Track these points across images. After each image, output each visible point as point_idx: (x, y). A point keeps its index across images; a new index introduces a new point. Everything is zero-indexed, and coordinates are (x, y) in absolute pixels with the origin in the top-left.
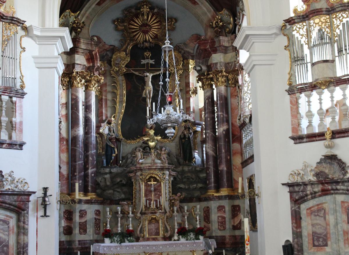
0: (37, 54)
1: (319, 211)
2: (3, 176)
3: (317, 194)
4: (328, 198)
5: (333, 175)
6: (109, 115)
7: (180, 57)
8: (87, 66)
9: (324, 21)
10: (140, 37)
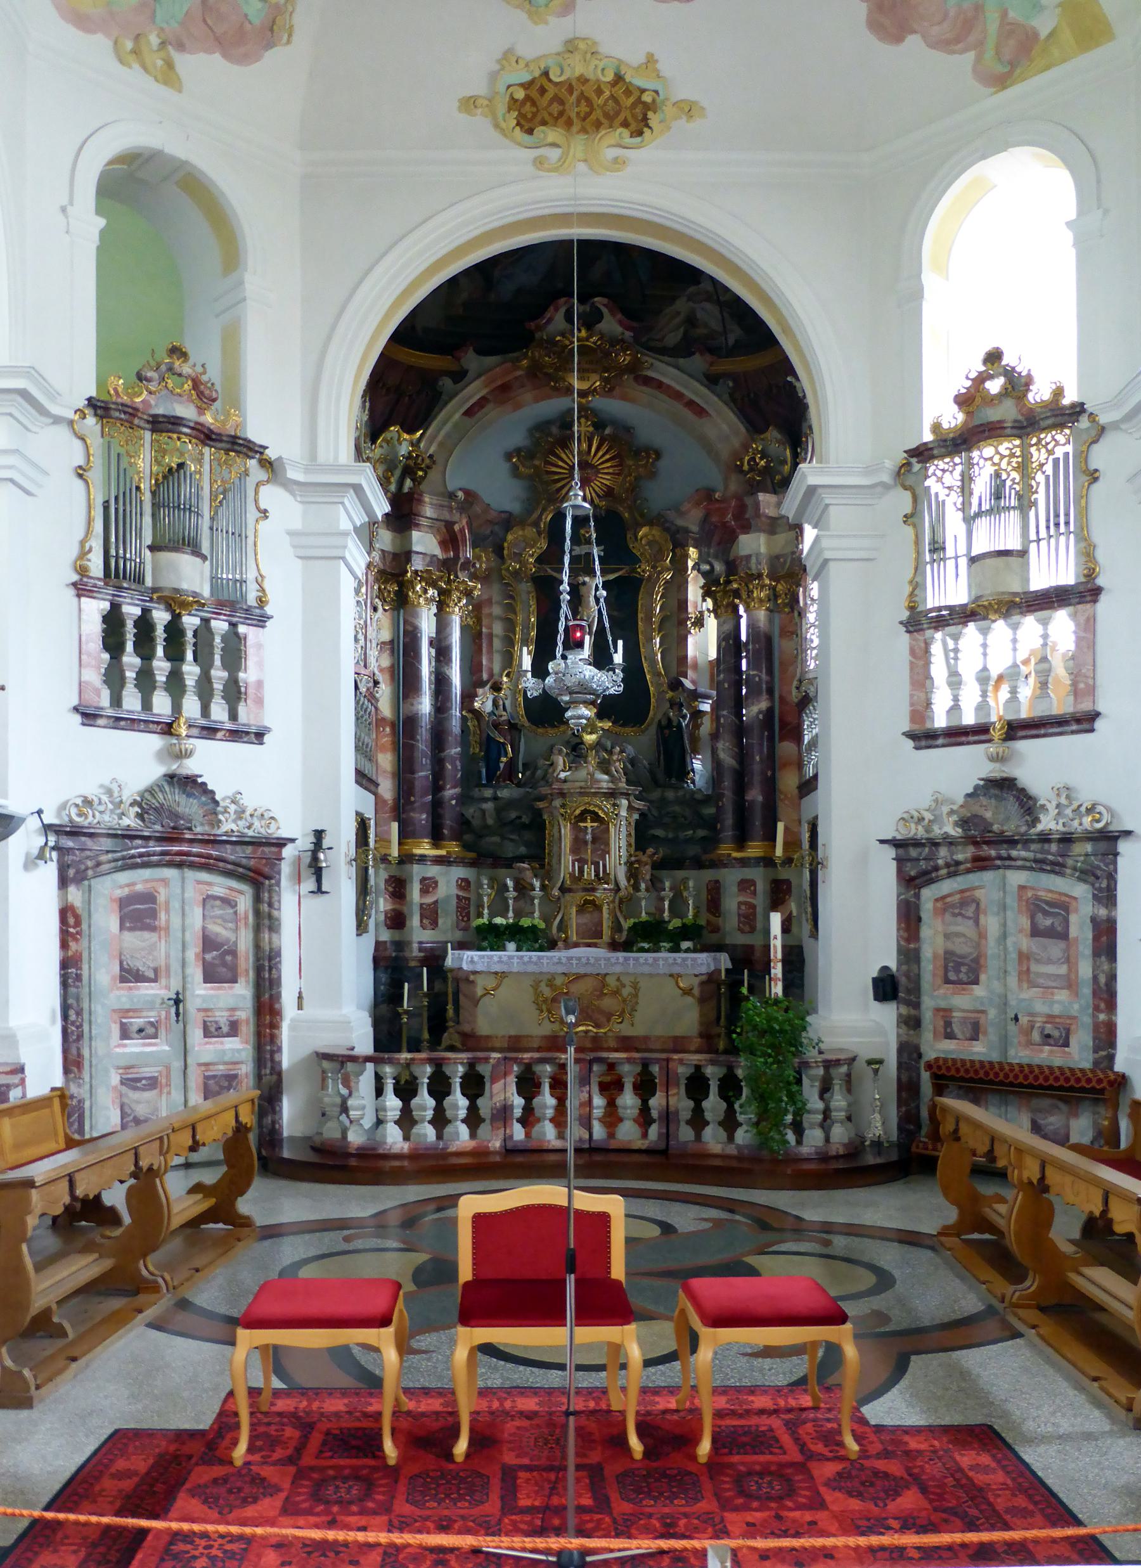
0: (297, 525)
2: (217, 803)
3: (962, 867)
4: (988, 876)
5: (1002, 825)
6: (496, 668)
7: (666, 541)
8: (440, 557)
9: (1007, 453)
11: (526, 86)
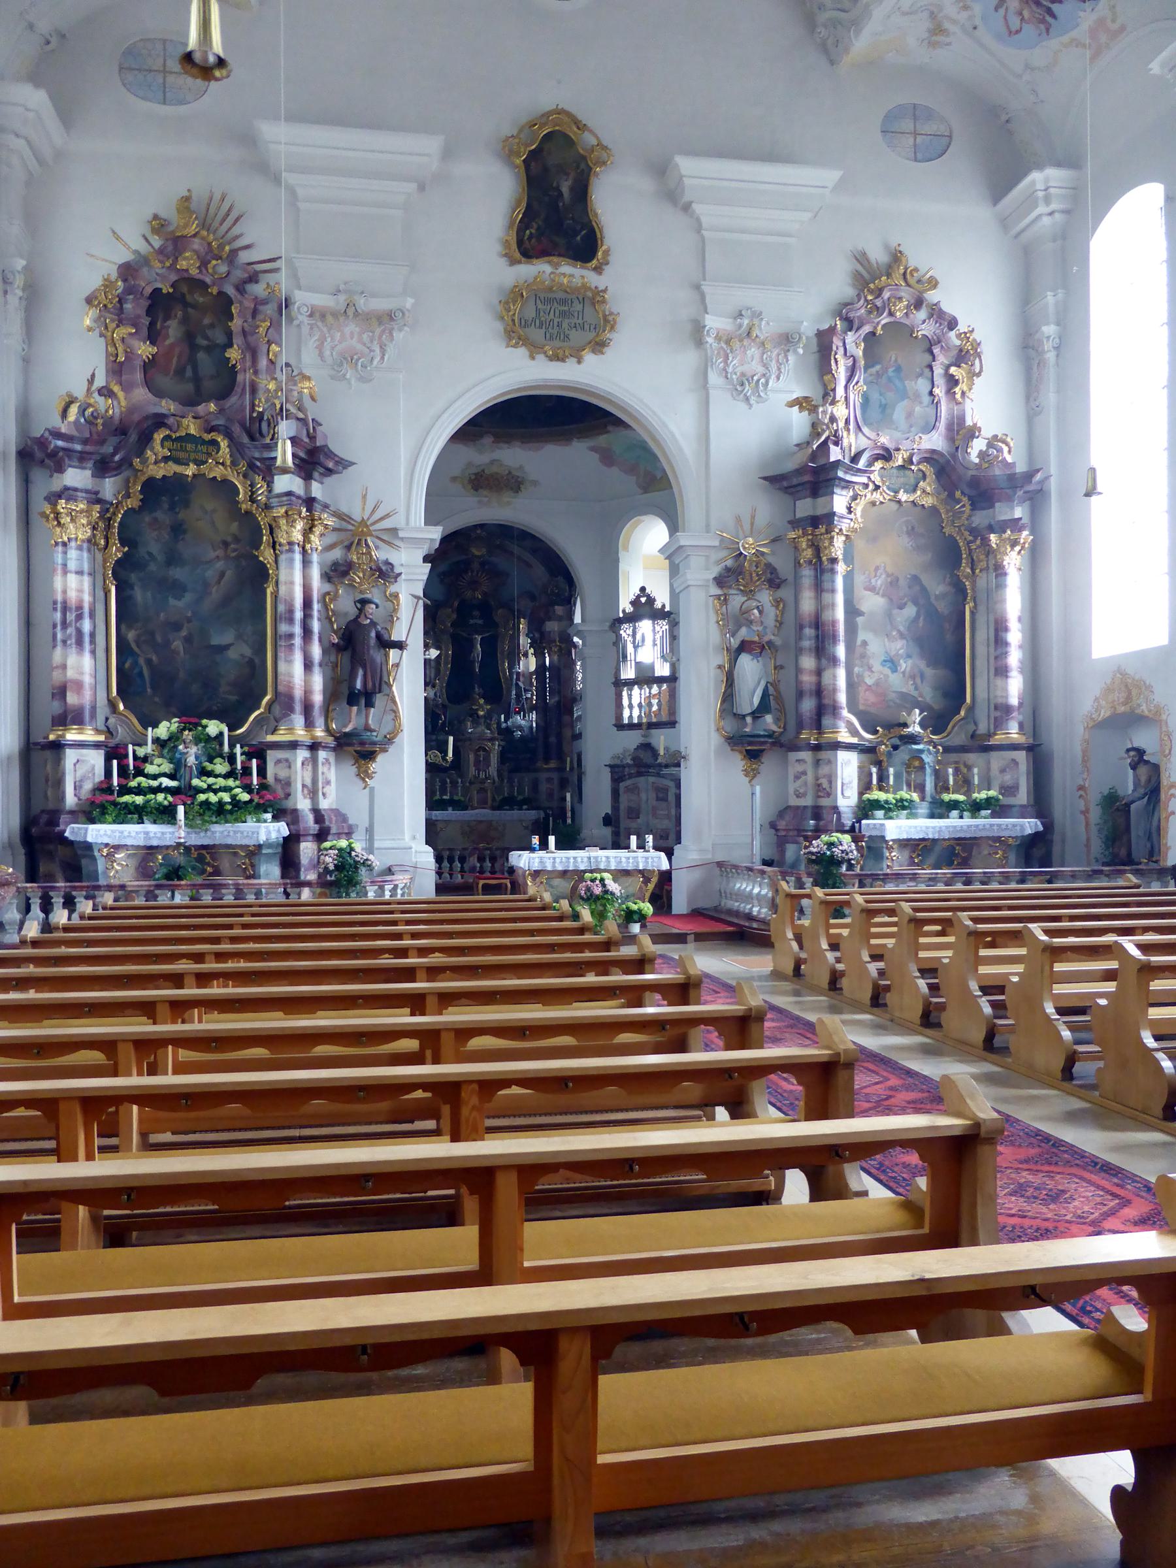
1: (634, 790)
4: (642, 779)
6: (433, 676)
10: (468, 594)
11: (475, 474)
